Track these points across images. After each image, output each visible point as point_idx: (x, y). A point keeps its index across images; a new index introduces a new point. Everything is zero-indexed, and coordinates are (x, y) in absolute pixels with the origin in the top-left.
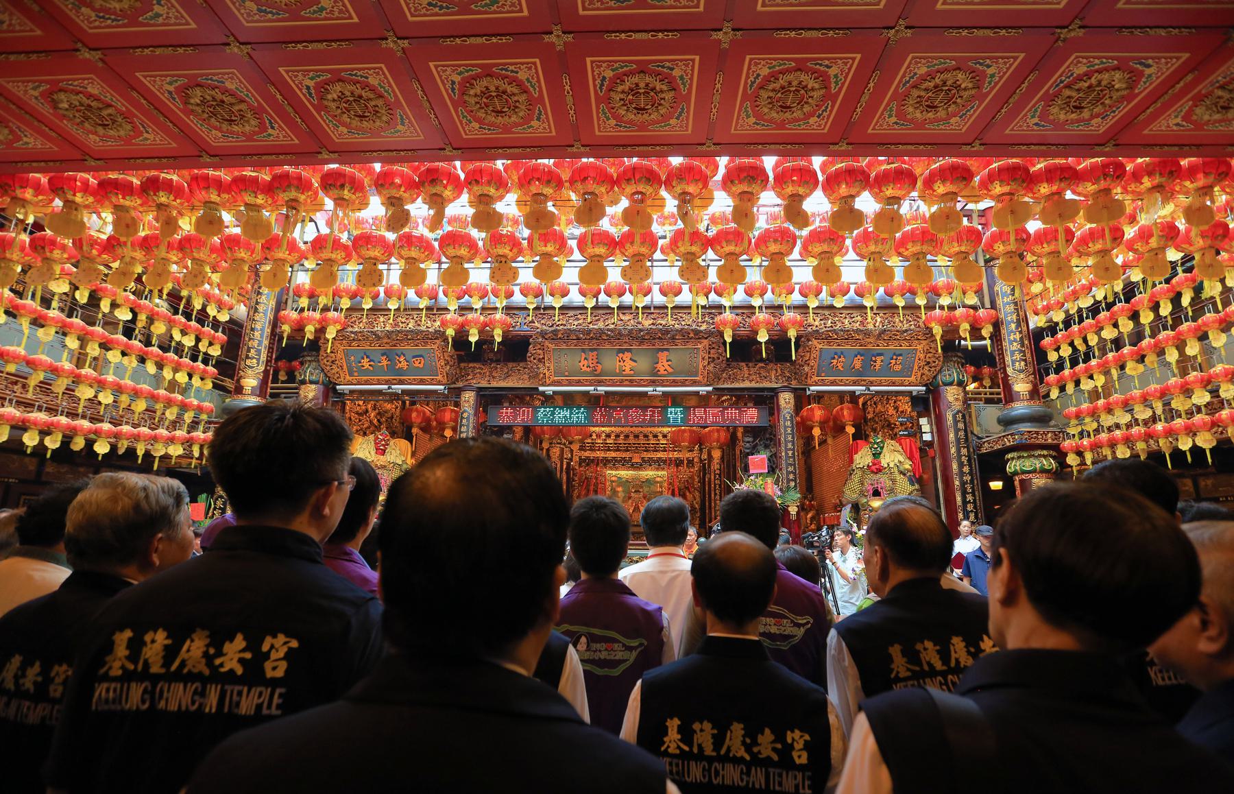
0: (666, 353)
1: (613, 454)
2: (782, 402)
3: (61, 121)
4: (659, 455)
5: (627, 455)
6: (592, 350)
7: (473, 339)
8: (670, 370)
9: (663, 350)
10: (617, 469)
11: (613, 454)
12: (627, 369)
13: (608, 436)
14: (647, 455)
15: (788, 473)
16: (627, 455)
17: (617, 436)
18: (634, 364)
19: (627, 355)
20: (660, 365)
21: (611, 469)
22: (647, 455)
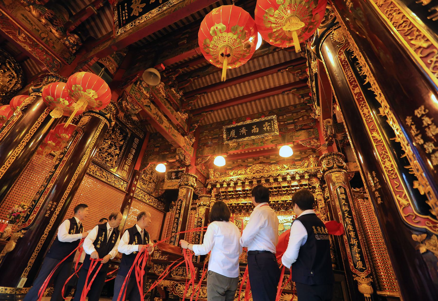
13: (302, 177)
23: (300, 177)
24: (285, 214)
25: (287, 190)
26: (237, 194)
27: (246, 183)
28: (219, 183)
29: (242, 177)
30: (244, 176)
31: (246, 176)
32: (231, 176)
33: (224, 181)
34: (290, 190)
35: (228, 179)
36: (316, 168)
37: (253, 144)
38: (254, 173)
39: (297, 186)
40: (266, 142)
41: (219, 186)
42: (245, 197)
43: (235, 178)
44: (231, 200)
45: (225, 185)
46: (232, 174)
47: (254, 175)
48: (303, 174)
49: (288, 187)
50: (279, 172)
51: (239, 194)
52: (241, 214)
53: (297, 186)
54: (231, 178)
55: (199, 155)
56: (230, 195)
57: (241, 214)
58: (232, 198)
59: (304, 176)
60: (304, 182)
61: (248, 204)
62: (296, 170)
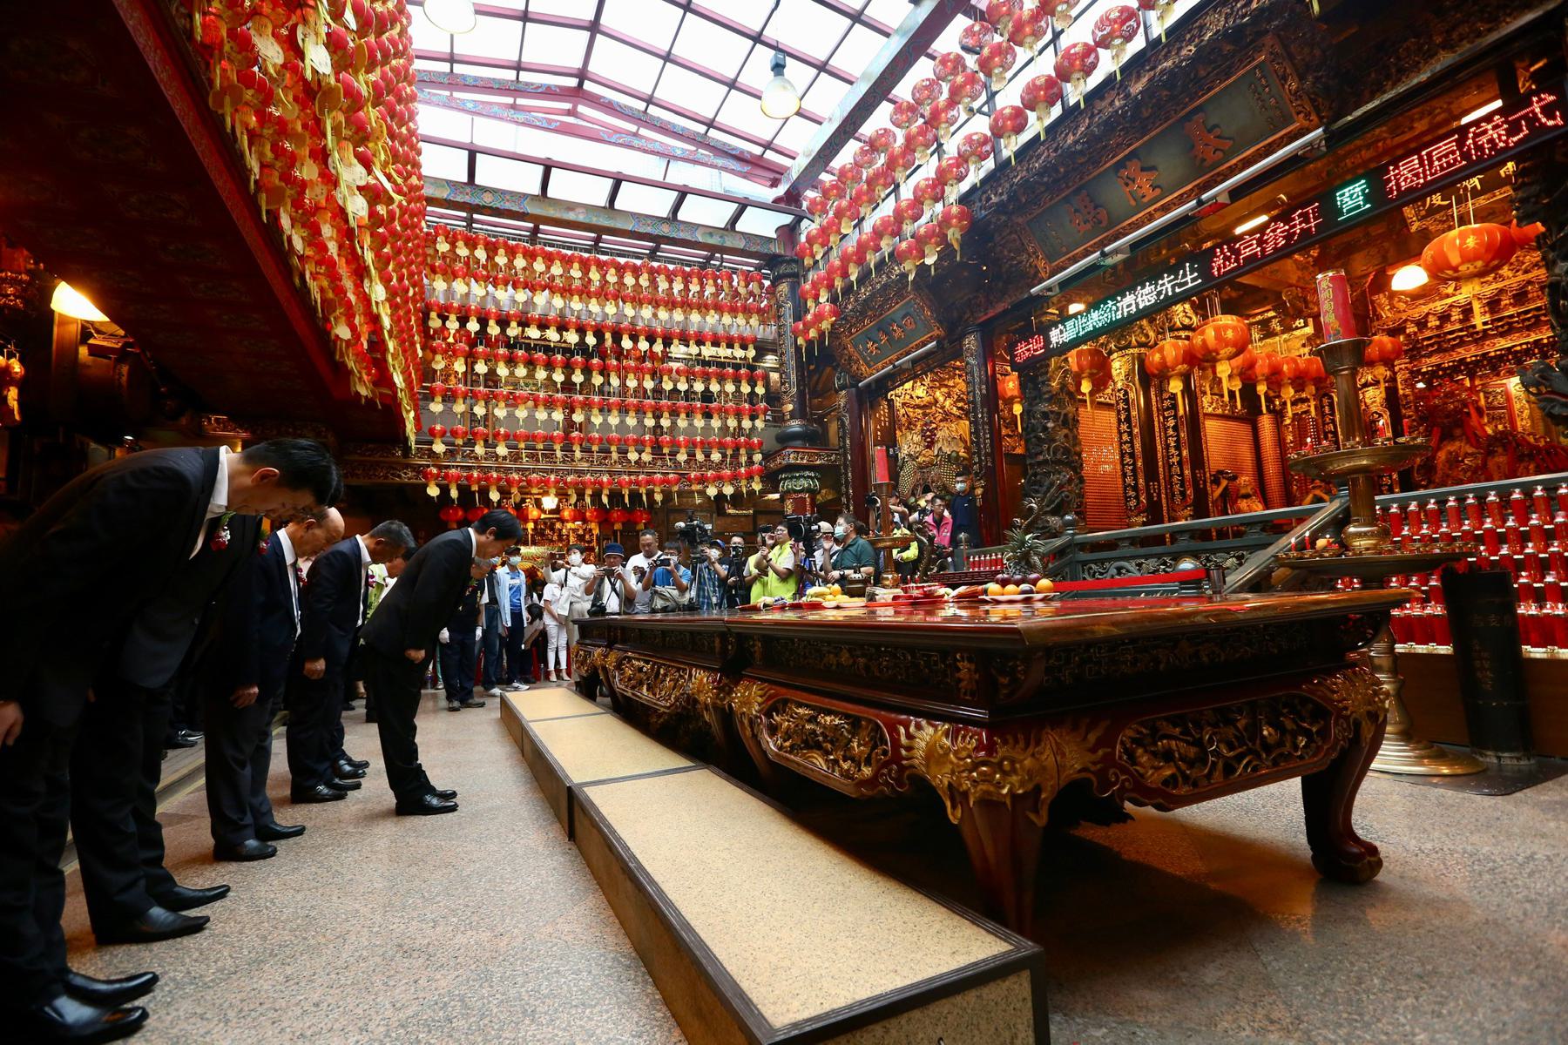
0: (1199, 117)
6: (1077, 191)
11: (1503, 343)
18: (1153, 176)
19: (1133, 167)
23: (1440, 318)
30: (1494, 286)
31: (1500, 285)
32: (1448, 296)
35: (1439, 306)
38: (1526, 272)
47: (1529, 276)
50: (1425, 309)
54: (1449, 301)
57: (1498, 375)
60: (1449, 327)
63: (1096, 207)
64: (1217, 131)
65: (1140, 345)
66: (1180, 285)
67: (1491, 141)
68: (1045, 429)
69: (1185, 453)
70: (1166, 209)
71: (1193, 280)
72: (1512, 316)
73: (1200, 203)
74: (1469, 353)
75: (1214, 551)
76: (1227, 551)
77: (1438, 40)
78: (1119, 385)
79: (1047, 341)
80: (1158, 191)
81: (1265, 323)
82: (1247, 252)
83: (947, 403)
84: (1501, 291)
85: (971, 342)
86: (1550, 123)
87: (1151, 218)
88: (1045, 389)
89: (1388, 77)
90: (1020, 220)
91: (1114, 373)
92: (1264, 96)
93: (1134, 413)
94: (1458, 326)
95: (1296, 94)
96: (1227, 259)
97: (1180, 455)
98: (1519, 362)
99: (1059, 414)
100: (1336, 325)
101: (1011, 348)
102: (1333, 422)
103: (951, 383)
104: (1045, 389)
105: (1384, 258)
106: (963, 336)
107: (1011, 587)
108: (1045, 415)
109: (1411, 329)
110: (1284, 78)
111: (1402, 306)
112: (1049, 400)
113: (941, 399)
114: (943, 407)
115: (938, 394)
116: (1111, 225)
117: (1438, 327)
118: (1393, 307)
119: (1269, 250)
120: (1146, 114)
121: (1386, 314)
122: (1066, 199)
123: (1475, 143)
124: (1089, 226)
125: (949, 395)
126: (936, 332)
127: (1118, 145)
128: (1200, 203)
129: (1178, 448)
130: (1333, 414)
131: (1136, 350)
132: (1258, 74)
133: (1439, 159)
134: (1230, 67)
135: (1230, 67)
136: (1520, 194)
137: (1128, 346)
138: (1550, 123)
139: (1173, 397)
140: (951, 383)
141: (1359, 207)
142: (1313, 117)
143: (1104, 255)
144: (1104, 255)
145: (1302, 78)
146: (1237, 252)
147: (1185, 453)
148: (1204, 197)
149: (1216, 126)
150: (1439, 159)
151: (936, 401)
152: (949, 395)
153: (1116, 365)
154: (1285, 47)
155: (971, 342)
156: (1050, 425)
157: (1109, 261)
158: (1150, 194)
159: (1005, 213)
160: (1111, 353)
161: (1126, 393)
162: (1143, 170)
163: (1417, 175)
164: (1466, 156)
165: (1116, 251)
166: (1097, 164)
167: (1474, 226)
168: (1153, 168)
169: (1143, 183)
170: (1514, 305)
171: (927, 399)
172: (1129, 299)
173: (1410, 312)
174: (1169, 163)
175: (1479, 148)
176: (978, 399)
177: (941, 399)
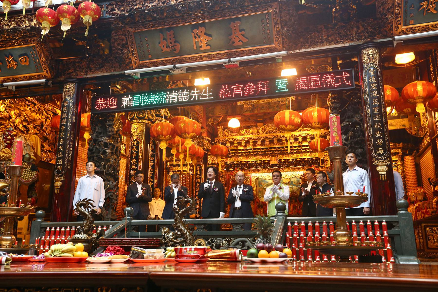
0: (238, 22)
1: (254, 159)
2: (365, 59)
3: (104, 235)
4: (294, 157)
5: (265, 159)
6: (169, 29)
7: (65, 27)
8: (245, 40)
9: (234, 20)
10: (259, 171)
11: (254, 159)
12: (204, 44)
13: (247, 142)
14: (282, 158)
15: (375, 131)
16: (265, 159)
17: (255, 142)
18: (209, 39)
19: (201, 31)
20: (234, 36)
21: (254, 171)
22: (282, 158)
23: (238, 143)
24: (294, 169)
25: (297, 149)
26: (247, 152)
27: (258, 143)
28: (229, 141)
29: (254, 136)
30: (256, 135)
31: (258, 136)
32: (242, 135)
33: (235, 140)
34: (300, 149)
35: (239, 138)
36: (326, 131)
37: (269, 108)
38: (266, 133)
39: (243, 150)
40: (282, 107)
41: (229, 145)
42: (255, 155)
43: (246, 137)
44: (241, 158)
45: (236, 144)
46: (243, 132)
47: (267, 135)
48: (248, 140)
49: (299, 146)
50: (235, 137)
51: (250, 152)
52: (250, 171)
53: (243, 150)
54: (242, 137)
55: (210, 115)
56: (240, 153)
57: (250, 171)
58: (242, 155)
59: (241, 143)
60: (240, 148)
61: (258, 162)
62: (308, 132)
63: (175, 42)
64: (243, 32)
65: (149, 119)
66: (203, 96)
67: (330, 82)
68: (104, 153)
69: (156, 181)
70: (210, 58)
71: (210, 96)
72: (259, 149)
73: (230, 61)
74: (243, 160)
75: (216, 236)
76: (223, 237)
77: (325, 37)
78: (135, 137)
79: (120, 102)
80: (209, 47)
81: (110, 126)
82: (236, 92)
83: (17, 121)
84: (258, 138)
85: (70, 88)
86: (347, 83)
87: (201, 59)
88: (110, 129)
89: (307, 42)
90: (131, 30)
91: (133, 130)
92: (266, 28)
93: (140, 155)
94: (242, 148)
95: (278, 32)
96: (226, 91)
97: (153, 182)
98: (272, 167)
99: (114, 146)
100: (338, 138)
101: (95, 99)
102: (200, 178)
103: (22, 108)
104: (110, 129)
105: (227, 112)
106: (65, 82)
107: (274, 253)
108: (106, 145)
109: (228, 145)
110: (276, 23)
111: (227, 134)
112: (109, 137)
113: (14, 117)
114: (14, 123)
115: (12, 113)
116: (180, 54)
117: (237, 147)
118: (223, 133)
119: (246, 94)
120: (216, 9)
121: (221, 135)
122: (161, 31)
123: (325, 81)
124: (168, 50)
125: (19, 115)
126: (44, 73)
127: (198, 17)
128: (230, 61)
129: (152, 178)
130: (200, 175)
131: (146, 121)
132: (267, 17)
133: (313, 82)
134: (258, 8)
135: (258, 8)
136: (333, 105)
137: (143, 118)
138: (347, 83)
139: (161, 150)
140: (22, 108)
141: (284, 89)
142: (281, 45)
143: (175, 67)
144: (175, 67)
145: (282, 27)
146: (232, 90)
147: (156, 181)
148: (232, 59)
149: (243, 30)
150: (313, 82)
151: (10, 117)
152: (19, 115)
153: (134, 126)
154: (281, 12)
155: (70, 88)
156: (108, 151)
157: (175, 72)
158: (204, 48)
159: (123, 22)
160: (133, 119)
161: (138, 143)
162: (205, 34)
163: (305, 84)
164: (322, 84)
165: (181, 68)
166: (184, 20)
167: (291, 110)
168: (210, 35)
169: (204, 41)
170: (260, 145)
171: (5, 114)
172: (174, 95)
173: (229, 137)
174: (217, 37)
175: (326, 83)
176: (69, 124)
177: (14, 117)
